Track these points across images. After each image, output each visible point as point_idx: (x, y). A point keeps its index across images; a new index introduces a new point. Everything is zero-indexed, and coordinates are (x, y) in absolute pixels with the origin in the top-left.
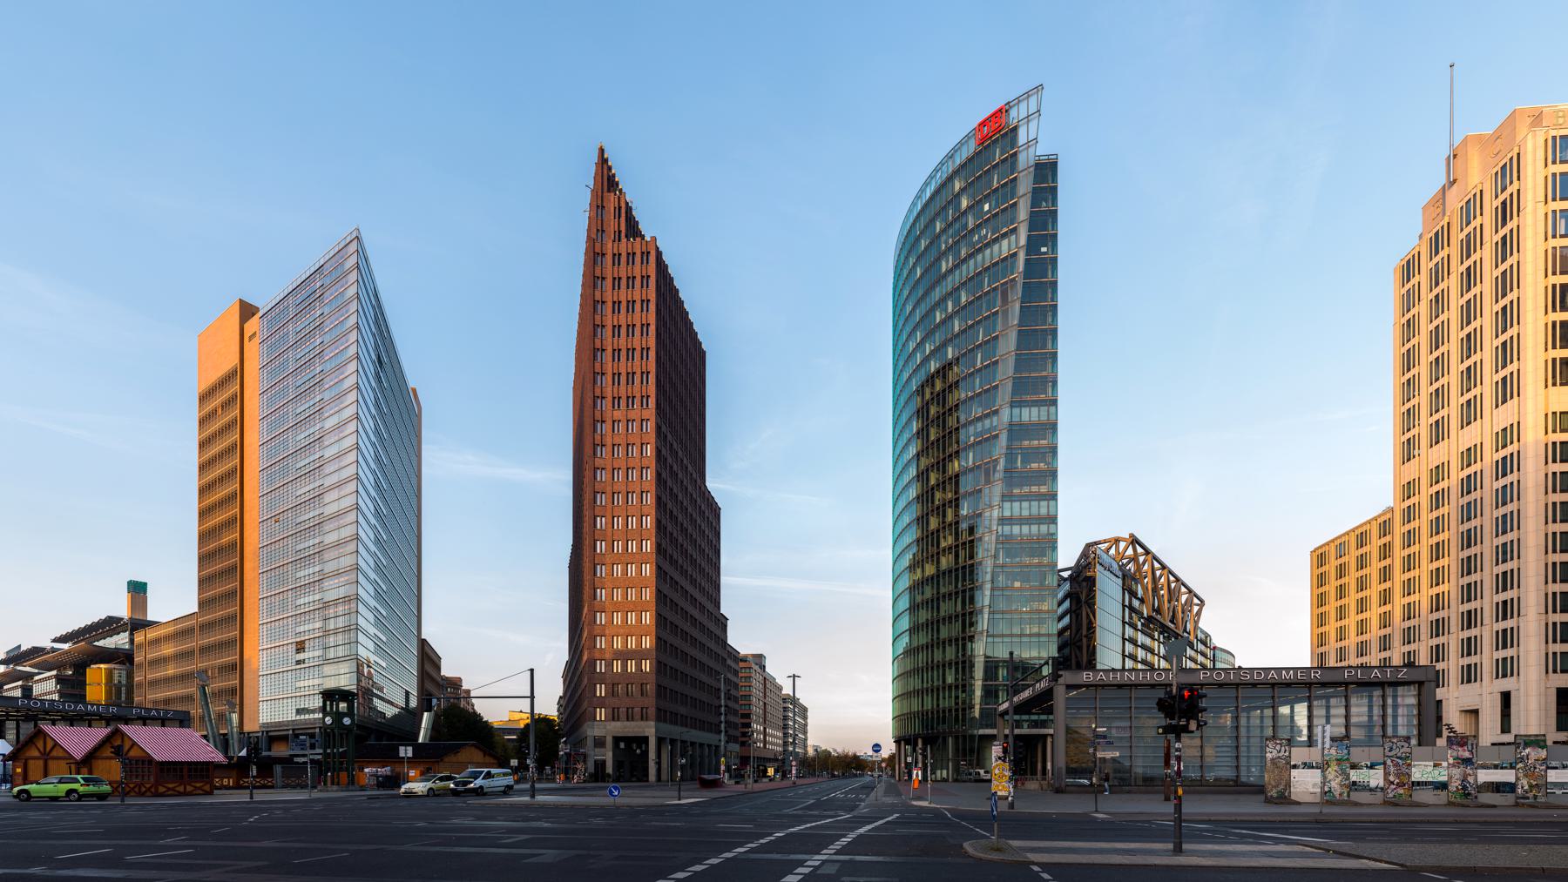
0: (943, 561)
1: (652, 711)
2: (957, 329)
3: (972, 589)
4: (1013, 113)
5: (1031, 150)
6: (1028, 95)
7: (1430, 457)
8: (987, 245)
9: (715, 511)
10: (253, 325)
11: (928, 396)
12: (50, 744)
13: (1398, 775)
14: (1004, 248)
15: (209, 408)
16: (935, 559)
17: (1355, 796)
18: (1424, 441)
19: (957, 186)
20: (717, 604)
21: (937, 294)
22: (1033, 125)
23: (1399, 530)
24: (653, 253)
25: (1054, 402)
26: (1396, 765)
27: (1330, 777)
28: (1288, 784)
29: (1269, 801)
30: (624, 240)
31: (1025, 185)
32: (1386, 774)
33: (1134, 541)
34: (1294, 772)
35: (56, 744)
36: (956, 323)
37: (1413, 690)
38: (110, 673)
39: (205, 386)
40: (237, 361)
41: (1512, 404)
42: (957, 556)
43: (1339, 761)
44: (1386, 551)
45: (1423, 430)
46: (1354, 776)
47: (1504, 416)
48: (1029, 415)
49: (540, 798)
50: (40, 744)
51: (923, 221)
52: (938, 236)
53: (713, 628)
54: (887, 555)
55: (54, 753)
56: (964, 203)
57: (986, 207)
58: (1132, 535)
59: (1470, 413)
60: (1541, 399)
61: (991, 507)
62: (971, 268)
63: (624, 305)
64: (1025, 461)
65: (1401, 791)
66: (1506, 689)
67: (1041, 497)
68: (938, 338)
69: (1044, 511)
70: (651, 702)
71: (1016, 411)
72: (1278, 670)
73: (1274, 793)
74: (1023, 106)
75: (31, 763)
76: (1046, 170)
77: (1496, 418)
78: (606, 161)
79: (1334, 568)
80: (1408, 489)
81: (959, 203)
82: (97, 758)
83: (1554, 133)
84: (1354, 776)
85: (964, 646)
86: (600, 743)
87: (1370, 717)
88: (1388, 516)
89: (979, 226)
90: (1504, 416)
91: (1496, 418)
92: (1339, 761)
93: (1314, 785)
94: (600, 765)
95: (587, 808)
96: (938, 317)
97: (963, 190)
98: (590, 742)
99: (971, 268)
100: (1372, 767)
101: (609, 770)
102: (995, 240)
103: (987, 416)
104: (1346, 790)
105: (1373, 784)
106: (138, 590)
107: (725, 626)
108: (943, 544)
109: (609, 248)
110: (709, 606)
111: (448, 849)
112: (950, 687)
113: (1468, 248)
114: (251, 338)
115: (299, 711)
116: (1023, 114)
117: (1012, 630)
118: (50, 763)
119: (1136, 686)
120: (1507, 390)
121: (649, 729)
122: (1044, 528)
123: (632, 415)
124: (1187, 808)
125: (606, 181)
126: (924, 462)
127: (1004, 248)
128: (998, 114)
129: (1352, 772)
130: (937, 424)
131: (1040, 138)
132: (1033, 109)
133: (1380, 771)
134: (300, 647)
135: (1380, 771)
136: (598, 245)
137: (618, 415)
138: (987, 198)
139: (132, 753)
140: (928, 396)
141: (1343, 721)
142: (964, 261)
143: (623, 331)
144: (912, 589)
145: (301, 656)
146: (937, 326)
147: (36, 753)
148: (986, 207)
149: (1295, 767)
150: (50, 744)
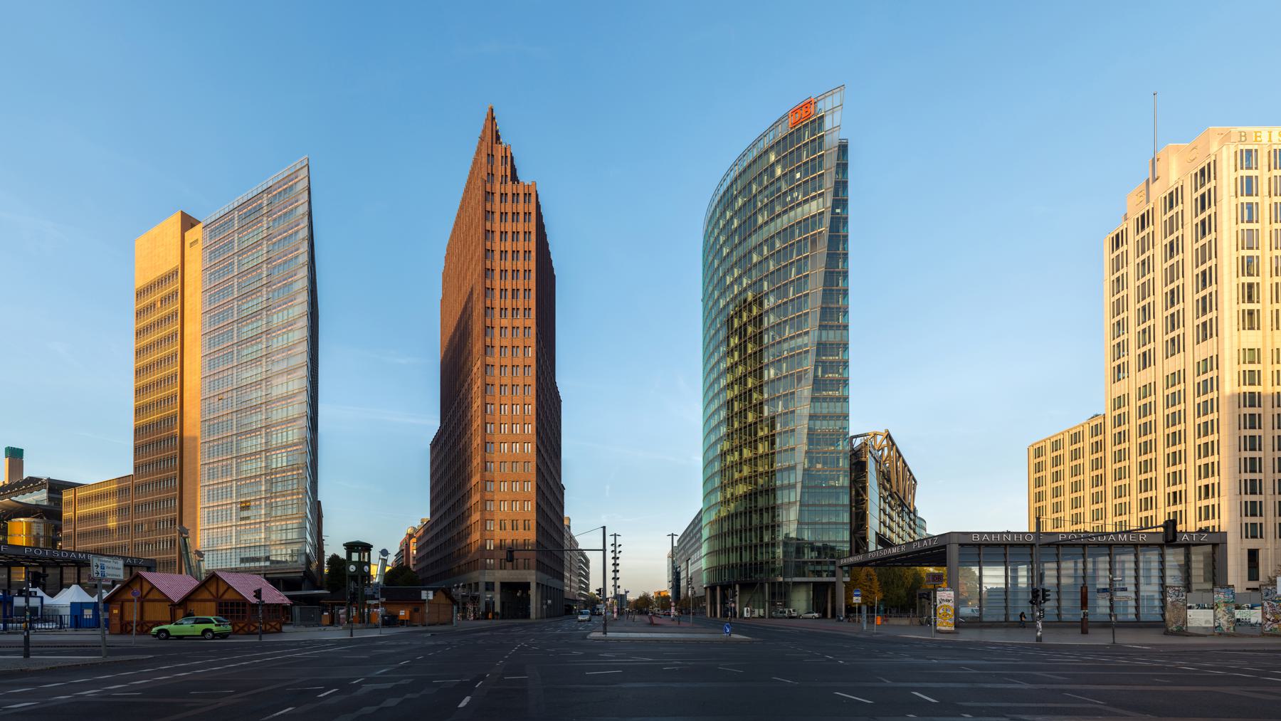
0: (760, 446)
1: (533, 562)
2: (772, 268)
4: (820, 105)
5: (836, 134)
7: (1136, 379)
8: (799, 205)
9: (434, 445)
10: (192, 234)
11: (745, 319)
12: (146, 588)
13: (1273, 614)
14: (813, 208)
16: (753, 445)
17: (1239, 629)
18: (1133, 367)
19: (773, 158)
21: (754, 240)
22: (837, 116)
23: (1110, 432)
24: (533, 195)
25: (846, 327)
26: (1272, 606)
27: (1219, 615)
28: (1185, 621)
29: (1168, 633)
30: (510, 183)
31: (830, 162)
32: (1264, 613)
33: (889, 437)
34: (1190, 612)
35: (153, 587)
38: (29, 526)
40: (179, 263)
41: (1211, 342)
43: (1226, 603)
44: (1098, 447)
45: (1132, 357)
46: (1238, 614)
47: (1206, 350)
48: (831, 336)
49: (609, 634)
50: (213, 589)
51: (739, 185)
55: (150, 597)
56: (779, 172)
57: (798, 176)
58: (887, 431)
59: (1174, 346)
60: (1235, 339)
62: (784, 221)
63: (510, 234)
64: (824, 372)
65: (1276, 626)
66: (1252, 547)
67: (838, 399)
68: (755, 274)
69: (838, 410)
70: (533, 556)
71: (824, 333)
72: (981, 534)
73: (1174, 628)
74: (828, 100)
75: (127, 604)
76: (843, 148)
77: (1196, 351)
78: (493, 119)
79: (1046, 462)
80: (1119, 402)
82: (192, 600)
83: (1242, 147)
84: (1238, 614)
86: (489, 586)
87: (1076, 570)
88: (1100, 420)
90: (1206, 350)
91: (1196, 351)
92: (1226, 603)
93: (1207, 622)
94: (490, 605)
95: (658, 641)
96: (755, 258)
97: (778, 162)
98: (482, 587)
99: (784, 221)
100: (1252, 608)
101: (498, 609)
102: (806, 201)
103: (799, 335)
104: (1232, 626)
105: (1253, 620)
106: (15, 456)
108: (760, 434)
109: (498, 189)
111: (1129, 688)
112: (767, 545)
113: (1171, 226)
114: (192, 245)
115: (243, 560)
116: (829, 107)
118: (147, 605)
119: (1012, 545)
120: (1206, 332)
121: (531, 576)
122: (839, 423)
123: (516, 323)
125: (493, 135)
127: (813, 208)
128: (808, 104)
129: (1237, 612)
130: (742, 337)
131: (836, 126)
132: (837, 103)
133: (1258, 611)
134: (245, 507)
135: (1258, 611)
136: (488, 185)
137: (505, 322)
139: (227, 596)
141: (1055, 573)
142: (779, 215)
143: (509, 255)
144: (723, 471)
145: (245, 514)
148: (798, 176)
149: (1190, 608)
150: (146, 588)
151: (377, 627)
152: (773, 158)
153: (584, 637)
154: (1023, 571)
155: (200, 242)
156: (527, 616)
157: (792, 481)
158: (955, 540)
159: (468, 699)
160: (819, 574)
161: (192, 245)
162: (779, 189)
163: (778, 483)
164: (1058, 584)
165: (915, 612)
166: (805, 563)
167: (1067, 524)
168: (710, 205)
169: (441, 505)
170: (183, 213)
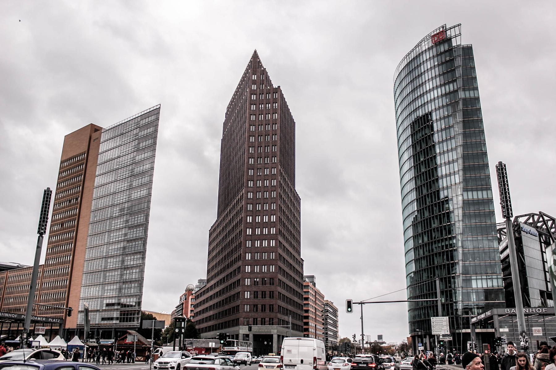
3: (452, 305)
39: (64, 158)
40: (86, 149)
53: (297, 267)
76: (468, 51)
107: (302, 265)
110: (296, 255)
114: (94, 140)
132: (457, 33)
156: (469, 333)
161: (94, 140)
163: (440, 175)
169: (216, 276)
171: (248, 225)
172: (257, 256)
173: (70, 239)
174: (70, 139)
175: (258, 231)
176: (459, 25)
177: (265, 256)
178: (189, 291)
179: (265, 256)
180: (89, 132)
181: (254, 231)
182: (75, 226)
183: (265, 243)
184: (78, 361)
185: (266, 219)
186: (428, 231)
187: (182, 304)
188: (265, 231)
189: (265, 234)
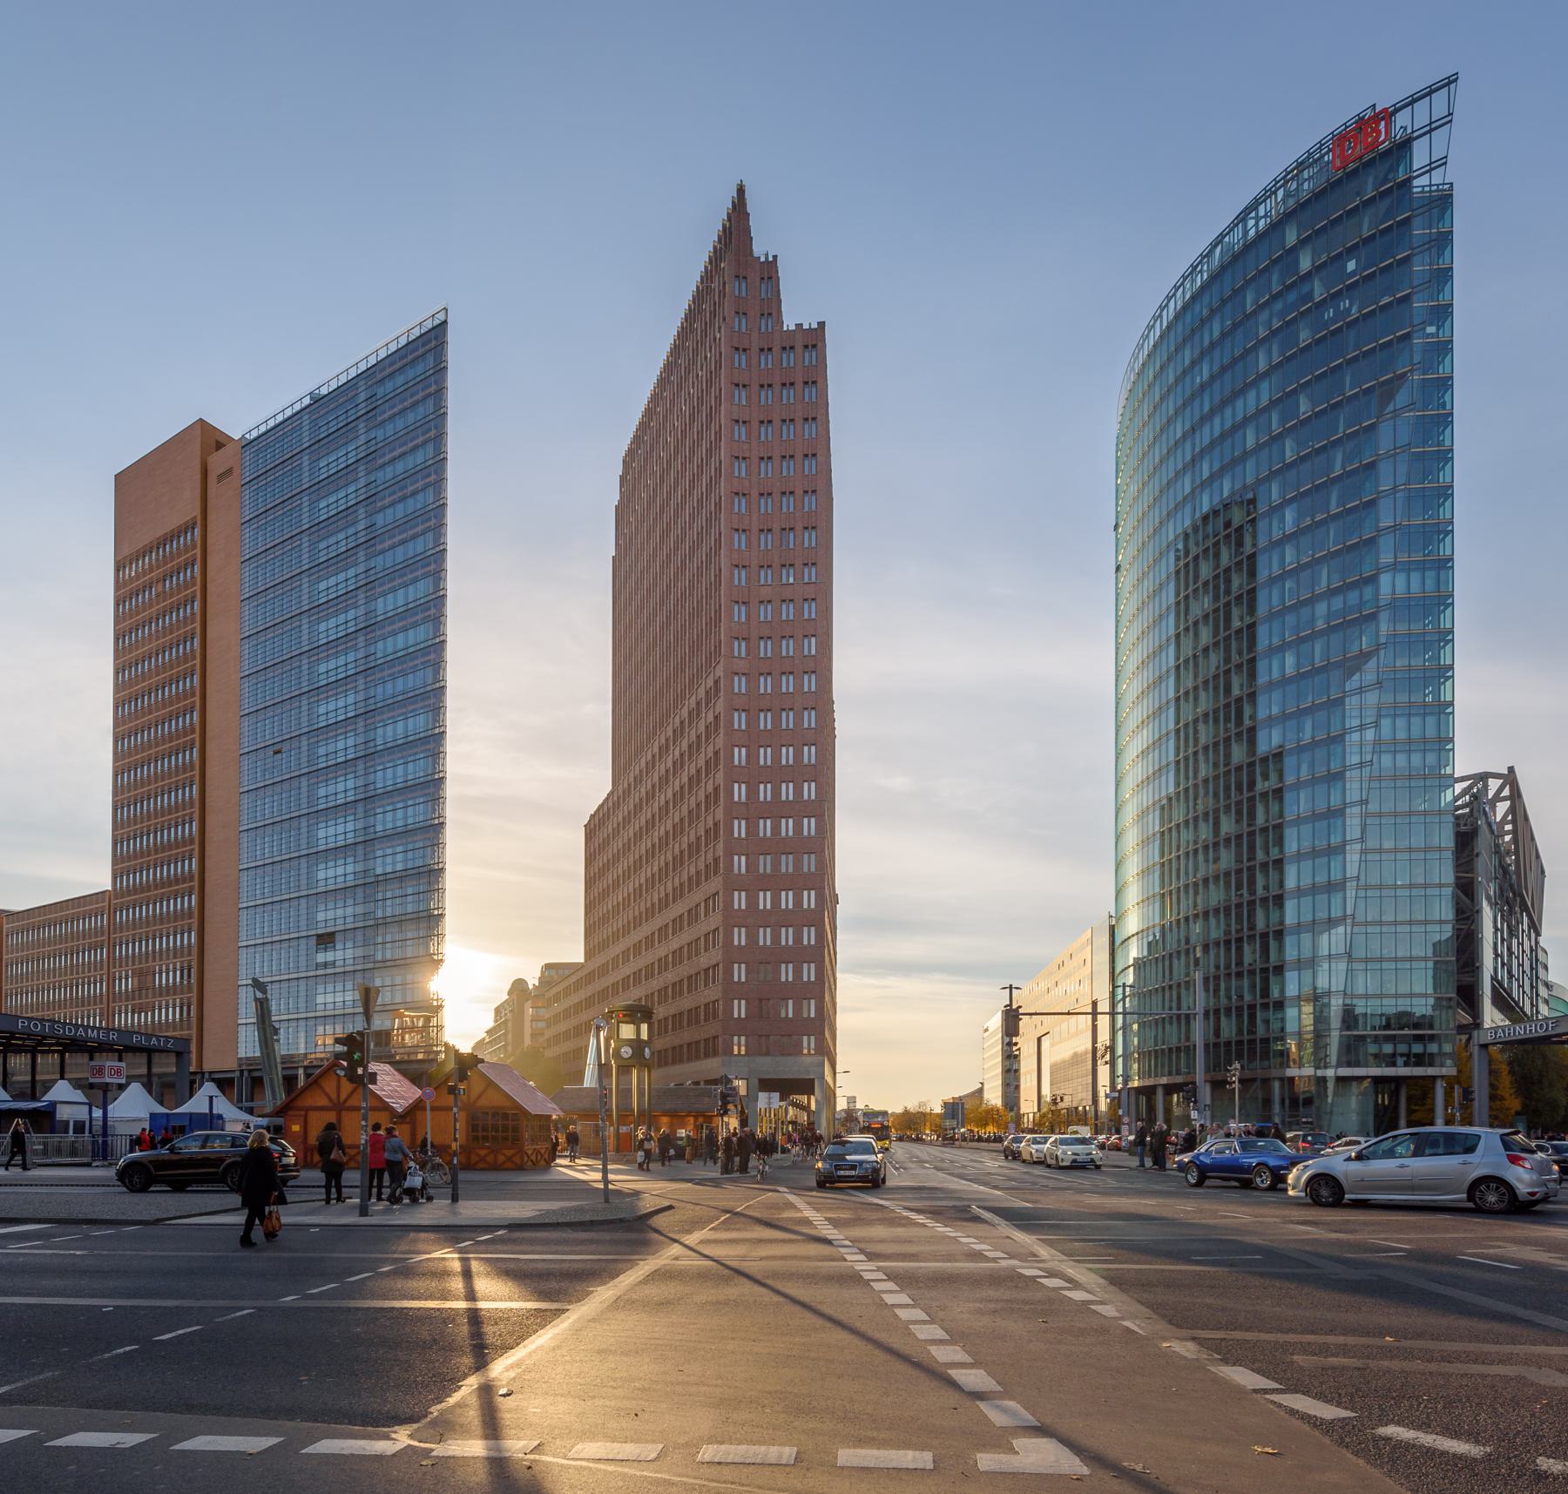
6: (1430, 92)
9: (593, 829)
10: (218, 462)
15: (600, 886)
19: (1291, 238)
20: (1246, 1366)
33: (1510, 778)
36: (1275, 277)
37: (143, 1059)
39: (126, 551)
40: (197, 513)
42: (1227, 650)
52: (1245, 455)
54: (448, 715)
56: (1305, 264)
61: (1124, 1013)
76: (1442, 201)
81: (1297, 262)
85: (1266, 981)
88: (441, 317)
89: (1336, 297)
97: (1303, 242)
114: (221, 477)
117: (1355, 958)
124: (598, 1176)
126: (1188, 712)
128: (1368, 123)
131: (1476, 169)
138: (1351, 251)
140: (1225, 559)
146: (1245, 455)
147: (323, 1102)
151: (1442, 1077)
152: (1291, 238)
153: (296, 1453)
154: (644, 1027)
155: (236, 472)
157: (1336, 875)
158: (1441, 1150)
159: (1391, 1430)
160: (1391, 1061)
161: (221, 477)
162: (1309, 296)
164: (33, 1081)
165: (1349, 1018)
166: (1363, 1038)
167: (1440, 1121)
168: (1135, 356)
170: (425, 353)
171: (733, 775)
172: (765, 865)
173: (184, 844)
174: (132, 485)
175: (765, 792)
176: (1451, 81)
177: (787, 864)
178: (519, 987)
179: (787, 864)
180: (196, 449)
181: (752, 792)
182: (191, 878)
183: (787, 827)
184: (1012, 1450)
185: (787, 755)
186: (1238, 803)
187: (505, 1022)
188: (787, 791)
189: (787, 801)
